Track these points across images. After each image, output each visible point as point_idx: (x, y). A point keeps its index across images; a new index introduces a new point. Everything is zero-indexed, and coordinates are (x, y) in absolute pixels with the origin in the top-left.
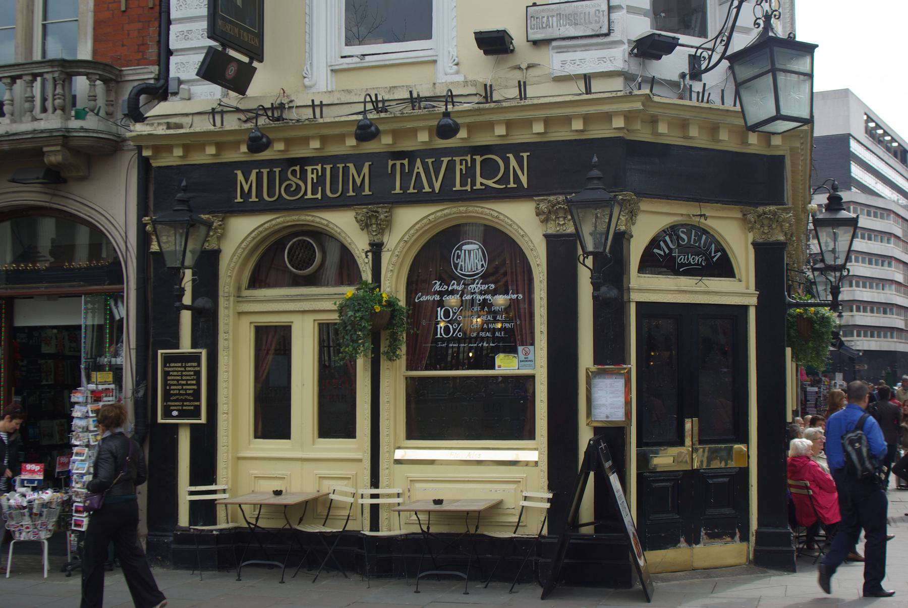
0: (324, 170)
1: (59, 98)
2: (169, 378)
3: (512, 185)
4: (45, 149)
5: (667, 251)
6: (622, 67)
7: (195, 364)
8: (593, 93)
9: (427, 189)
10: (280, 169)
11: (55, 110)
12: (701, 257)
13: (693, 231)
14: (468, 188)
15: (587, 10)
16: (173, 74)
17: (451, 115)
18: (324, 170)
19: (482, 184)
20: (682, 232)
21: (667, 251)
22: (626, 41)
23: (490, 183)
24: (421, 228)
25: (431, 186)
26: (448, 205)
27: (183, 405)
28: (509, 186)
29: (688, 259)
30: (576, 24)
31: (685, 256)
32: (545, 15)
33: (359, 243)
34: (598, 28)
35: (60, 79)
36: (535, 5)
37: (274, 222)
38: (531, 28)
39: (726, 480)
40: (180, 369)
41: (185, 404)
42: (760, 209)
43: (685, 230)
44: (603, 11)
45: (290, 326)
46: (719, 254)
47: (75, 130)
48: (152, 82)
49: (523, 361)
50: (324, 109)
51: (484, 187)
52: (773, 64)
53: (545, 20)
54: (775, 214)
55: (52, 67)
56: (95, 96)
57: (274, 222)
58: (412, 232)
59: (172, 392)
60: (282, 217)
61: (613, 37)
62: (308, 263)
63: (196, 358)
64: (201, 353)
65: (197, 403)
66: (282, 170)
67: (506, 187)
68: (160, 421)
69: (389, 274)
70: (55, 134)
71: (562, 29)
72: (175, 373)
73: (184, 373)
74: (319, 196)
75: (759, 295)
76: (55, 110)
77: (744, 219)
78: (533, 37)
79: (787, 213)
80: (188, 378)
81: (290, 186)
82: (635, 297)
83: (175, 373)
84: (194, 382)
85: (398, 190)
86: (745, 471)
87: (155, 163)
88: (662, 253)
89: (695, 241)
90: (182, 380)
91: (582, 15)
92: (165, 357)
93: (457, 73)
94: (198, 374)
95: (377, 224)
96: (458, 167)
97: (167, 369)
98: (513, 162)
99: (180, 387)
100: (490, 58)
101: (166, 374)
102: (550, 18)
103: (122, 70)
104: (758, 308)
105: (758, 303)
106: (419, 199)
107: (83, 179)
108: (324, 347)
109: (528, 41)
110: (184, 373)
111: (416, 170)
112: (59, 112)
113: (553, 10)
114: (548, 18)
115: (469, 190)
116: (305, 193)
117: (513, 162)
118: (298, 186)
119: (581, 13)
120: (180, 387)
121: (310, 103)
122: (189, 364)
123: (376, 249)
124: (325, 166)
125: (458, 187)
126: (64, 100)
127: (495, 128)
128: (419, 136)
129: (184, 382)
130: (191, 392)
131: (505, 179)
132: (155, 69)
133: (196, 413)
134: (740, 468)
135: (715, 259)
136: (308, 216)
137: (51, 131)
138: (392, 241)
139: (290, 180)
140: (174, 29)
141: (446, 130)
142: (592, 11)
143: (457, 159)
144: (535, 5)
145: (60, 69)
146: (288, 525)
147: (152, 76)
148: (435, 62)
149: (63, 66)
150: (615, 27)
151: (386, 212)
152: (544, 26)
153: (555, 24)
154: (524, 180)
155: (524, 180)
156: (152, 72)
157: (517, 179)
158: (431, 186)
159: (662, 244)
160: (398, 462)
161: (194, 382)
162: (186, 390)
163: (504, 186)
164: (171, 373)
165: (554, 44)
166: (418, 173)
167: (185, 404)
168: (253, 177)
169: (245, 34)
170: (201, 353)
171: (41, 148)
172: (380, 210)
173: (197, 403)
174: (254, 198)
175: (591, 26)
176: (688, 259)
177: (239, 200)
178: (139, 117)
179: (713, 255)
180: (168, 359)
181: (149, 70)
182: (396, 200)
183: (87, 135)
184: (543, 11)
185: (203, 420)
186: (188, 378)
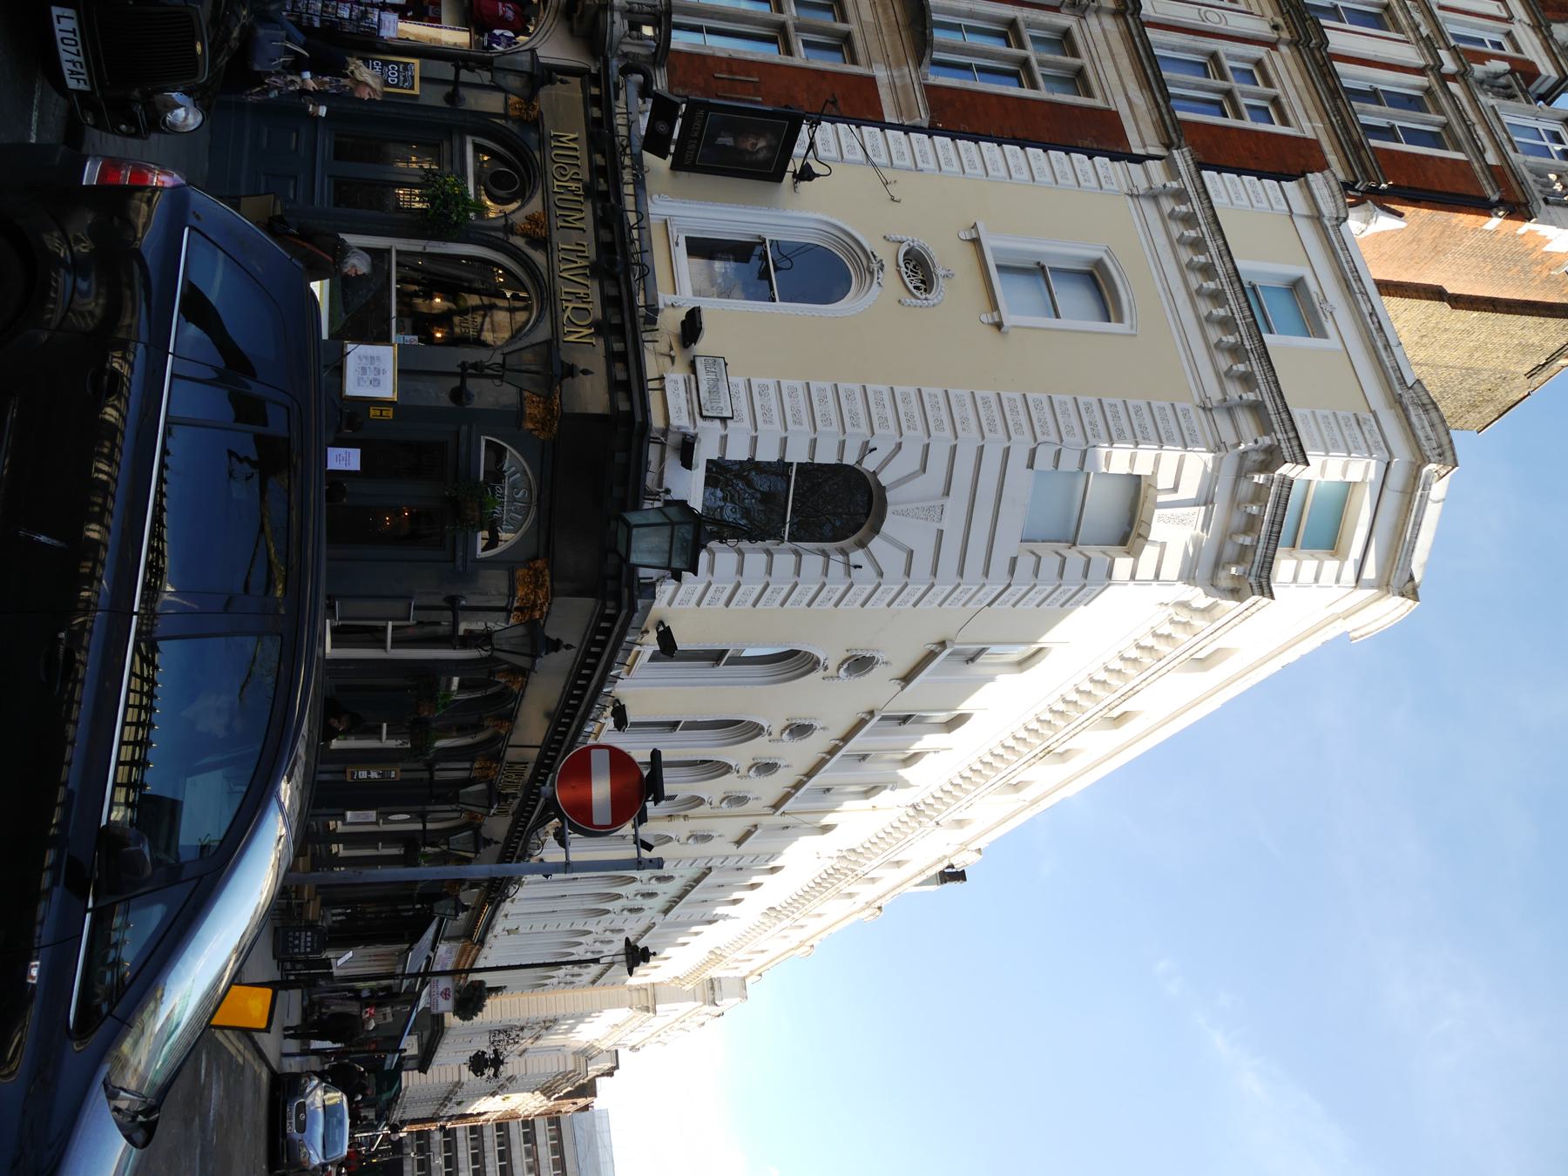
0: (579, 195)
19: (567, 307)
22: (697, 430)
23: (568, 312)
25: (565, 270)
36: (726, 364)
47: (612, 16)
48: (655, 88)
52: (678, 523)
54: (543, 585)
71: (705, 382)
74: (556, 190)
78: (698, 361)
93: (665, 305)
96: (582, 291)
98: (586, 332)
100: (678, 329)
107: (571, 31)
108: (420, 732)
116: (558, 180)
117: (586, 332)
118: (566, 175)
140: (761, 457)
144: (726, 364)
147: (659, 87)
150: (707, 424)
155: (571, 338)
158: (565, 270)
165: (693, 376)
166: (576, 262)
168: (572, 145)
177: (552, 134)
184: (721, 369)
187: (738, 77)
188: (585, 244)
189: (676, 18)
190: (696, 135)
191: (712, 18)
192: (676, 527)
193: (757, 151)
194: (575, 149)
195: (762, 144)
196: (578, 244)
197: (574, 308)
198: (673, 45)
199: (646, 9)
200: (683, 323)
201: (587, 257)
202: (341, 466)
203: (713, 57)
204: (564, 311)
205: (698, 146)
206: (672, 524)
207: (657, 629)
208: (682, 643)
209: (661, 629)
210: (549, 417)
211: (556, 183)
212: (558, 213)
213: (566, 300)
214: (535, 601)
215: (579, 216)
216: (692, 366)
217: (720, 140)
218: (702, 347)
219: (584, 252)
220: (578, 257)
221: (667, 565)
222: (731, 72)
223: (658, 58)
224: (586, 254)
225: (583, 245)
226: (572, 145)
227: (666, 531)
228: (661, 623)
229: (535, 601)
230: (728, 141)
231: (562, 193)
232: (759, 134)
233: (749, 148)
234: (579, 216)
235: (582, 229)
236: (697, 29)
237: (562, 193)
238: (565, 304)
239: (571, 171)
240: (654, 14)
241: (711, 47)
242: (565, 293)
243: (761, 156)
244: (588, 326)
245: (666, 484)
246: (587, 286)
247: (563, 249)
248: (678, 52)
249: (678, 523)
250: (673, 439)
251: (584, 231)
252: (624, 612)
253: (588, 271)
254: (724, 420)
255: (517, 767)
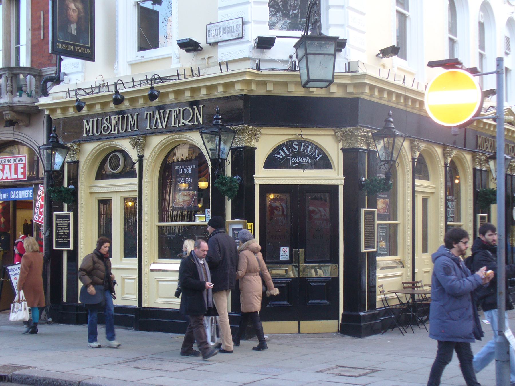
1: (9, 87)
2: (58, 226)
3: (196, 123)
4: (4, 113)
5: (284, 156)
6: (248, 55)
7: (68, 220)
8: (201, 76)
9: (160, 127)
10: (203, 106)
11: (7, 92)
12: (308, 158)
13: (303, 144)
14: (177, 125)
15: (232, 25)
16: (62, 71)
17: (155, 88)
18: (119, 118)
19: (183, 123)
20: (295, 144)
21: (284, 156)
23: (186, 122)
24: (160, 147)
25: (162, 125)
26: (170, 134)
27: (63, 240)
28: (194, 124)
29: (298, 159)
30: (228, 33)
31: (296, 158)
32: (214, 29)
33: (134, 155)
34: (238, 34)
35: (9, 77)
36: (211, 24)
37: (100, 146)
38: (209, 37)
39: (324, 284)
40: (62, 222)
41: (64, 239)
42: (344, 129)
43: (297, 143)
44: (240, 25)
45: (112, 199)
46: (321, 156)
48: (54, 75)
49: (208, 217)
50: (70, 92)
51: (183, 125)
53: (214, 31)
55: (5, 71)
56: (26, 85)
57: (167, 139)
58: (156, 149)
59: (59, 234)
60: (171, 136)
61: (245, 39)
62: (117, 166)
63: (67, 216)
64: (70, 214)
65: (69, 239)
66: (204, 106)
67: (193, 124)
68: (54, 248)
69: (147, 172)
70: (5, 105)
71: (222, 36)
72: (60, 224)
73: (64, 224)
74: (116, 132)
75: (345, 178)
76: (7, 92)
77: (335, 136)
78: (212, 40)
79: (358, 131)
80: (65, 226)
81: (105, 127)
82: (258, 182)
83: (60, 224)
84: (67, 229)
85: (148, 128)
86: (337, 279)
87: (53, 117)
88: (281, 157)
89: (304, 149)
90: (63, 227)
91: (231, 28)
92: (56, 216)
94: (69, 224)
95: (140, 146)
96: (173, 114)
97: (57, 222)
98: (196, 111)
99: (62, 231)
100: (191, 54)
101: (57, 224)
102: (217, 31)
103: (41, 70)
104: (345, 186)
105: (344, 183)
106: (91, 140)
109: (207, 44)
110: (64, 224)
111: (156, 117)
112: (9, 93)
113: (218, 26)
114: (216, 30)
115: (178, 126)
116: (111, 131)
117: (196, 111)
118: (108, 126)
119: (230, 27)
120: (62, 231)
121: (114, 84)
122: (66, 220)
123: (141, 158)
124: (119, 116)
125: (173, 125)
126: (12, 87)
127: (139, 100)
128: (186, 94)
129: (64, 229)
130: (66, 233)
131: (192, 120)
132: (55, 68)
133: (68, 245)
134: (333, 278)
135: (317, 159)
136: (114, 142)
137: (4, 104)
138: (147, 154)
139: (105, 124)
141: (79, 108)
142: (235, 25)
143: (173, 110)
144: (211, 24)
145: (8, 72)
146: (422, 295)
147: (53, 72)
148: (171, 57)
149: (9, 70)
151: (142, 139)
152: (214, 35)
153: (219, 33)
154: (201, 120)
155: (201, 120)
156: (53, 70)
157: (198, 120)
158: (162, 125)
159: (280, 151)
160: (152, 270)
161: (67, 229)
162: (64, 232)
163: (192, 124)
164: (59, 224)
166: (157, 118)
167: (64, 239)
168: (90, 123)
169: (79, 48)
170: (70, 214)
171: (2, 112)
172: (140, 138)
173: (69, 239)
174: (91, 134)
175: (234, 34)
176: (298, 159)
177: (85, 135)
178: (45, 94)
179: (316, 156)
180: (58, 217)
181: (52, 70)
182: (155, 132)
183: (20, 104)
185: (71, 248)
186: (65, 226)
187: (42, 24)
188: (146, 113)
189: (13, 65)
190: (72, 47)
191: (10, 41)
192: (308, 51)
193: (78, 8)
194: (93, 121)
195: (72, 6)
196: (147, 118)
197: (183, 119)
198: (29, 66)
199: (9, 83)
200: (187, 51)
201: (154, 112)
202: (282, 253)
203: (32, 40)
204: (185, 125)
205: (78, 46)
206: (306, 54)
207: (382, 58)
208: (393, 43)
209: (381, 55)
210: (247, 132)
211: (113, 132)
212: (129, 130)
213: (179, 123)
214: (361, 136)
215: (130, 118)
216: (214, 45)
217: (74, 32)
218: (201, 39)
219: (150, 114)
220: (154, 117)
221: (333, 57)
222: (39, 29)
223: (37, 74)
224: (152, 112)
225: (147, 114)
226: (90, 123)
227: (310, 57)
228: (377, 55)
229: (361, 136)
230: (73, 28)
231: (118, 128)
232: (67, 8)
233: (76, 14)
234: (130, 118)
235: (138, 115)
236: (18, 50)
237: (118, 128)
238: (181, 124)
239: (107, 124)
240: (12, 78)
241: (27, 41)
242: (175, 124)
243: (80, 6)
244: (193, 109)
245: (286, 58)
246: (170, 111)
247: (150, 127)
248: (32, 62)
249: (306, 51)
250: (256, 55)
251: (139, 114)
252: (366, 81)
253: (161, 111)
254: (243, 23)
255: (480, 141)
